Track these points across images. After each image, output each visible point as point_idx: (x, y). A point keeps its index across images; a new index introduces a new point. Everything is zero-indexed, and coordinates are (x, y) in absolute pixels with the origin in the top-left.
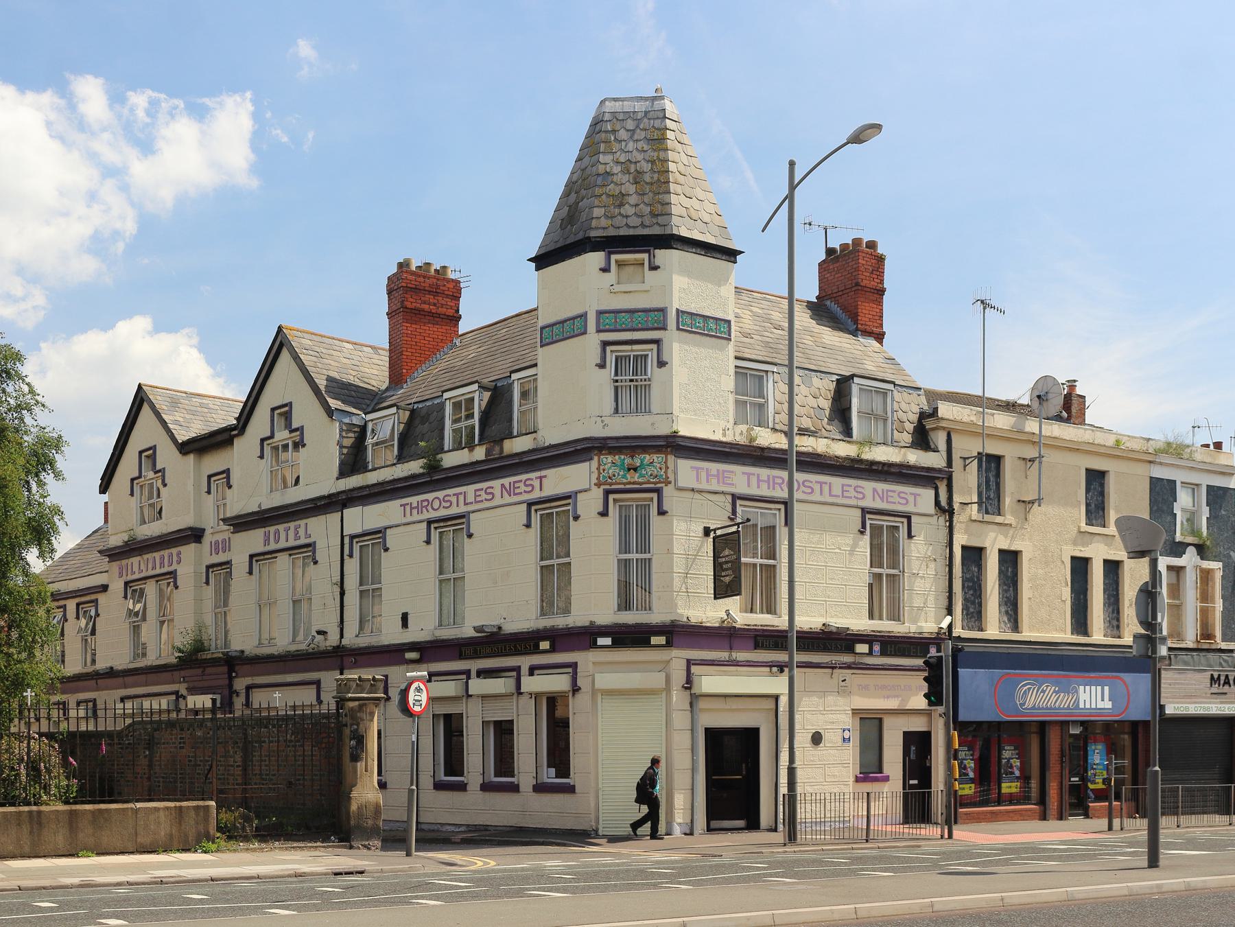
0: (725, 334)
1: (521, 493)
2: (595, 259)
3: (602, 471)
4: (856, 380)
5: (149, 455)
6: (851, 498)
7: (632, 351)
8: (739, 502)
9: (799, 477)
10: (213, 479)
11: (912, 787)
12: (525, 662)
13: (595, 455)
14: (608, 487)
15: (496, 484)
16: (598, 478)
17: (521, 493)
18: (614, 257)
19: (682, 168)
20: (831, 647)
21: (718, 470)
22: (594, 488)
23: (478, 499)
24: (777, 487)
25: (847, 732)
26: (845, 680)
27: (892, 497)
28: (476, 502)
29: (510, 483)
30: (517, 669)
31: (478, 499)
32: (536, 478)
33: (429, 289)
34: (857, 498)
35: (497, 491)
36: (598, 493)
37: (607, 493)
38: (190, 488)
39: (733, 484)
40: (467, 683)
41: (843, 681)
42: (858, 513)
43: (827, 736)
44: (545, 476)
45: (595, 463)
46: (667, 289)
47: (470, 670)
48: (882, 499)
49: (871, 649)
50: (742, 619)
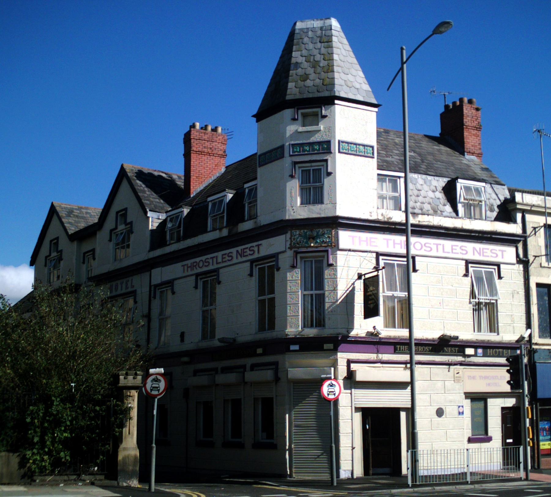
0: (370, 153)
1: (247, 256)
2: (288, 113)
3: (293, 240)
4: (459, 180)
5: (55, 242)
6: (458, 253)
10: (87, 255)
11: (509, 444)
12: (249, 361)
13: (289, 230)
14: (296, 249)
15: (234, 250)
16: (290, 244)
17: (247, 256)
18: (300, 111)
19: (342, 58)
20: (448, 351)
21: (367, 238)
22: (288, 251)
23: (224, 260)
25: (461, 408)
27: (456, 249)
28: (223, 262)
29: (241, 249)
30: (244, 367)
31: (224, 260)
32: (256, 246)
33: (207, 140)
34: (463, 254)
35: (234, 255)
36: (290, 253)
37: (297, 253)
38: (74, 261)
40: (244, 374)
42: (463, 263)
43: (448, 411)
44: (261, 245)
45: (288, 235)
46: (331, 129)
47: (217, 368)
48: (480, 254)
49: (476, 352)
50: (386, 333)
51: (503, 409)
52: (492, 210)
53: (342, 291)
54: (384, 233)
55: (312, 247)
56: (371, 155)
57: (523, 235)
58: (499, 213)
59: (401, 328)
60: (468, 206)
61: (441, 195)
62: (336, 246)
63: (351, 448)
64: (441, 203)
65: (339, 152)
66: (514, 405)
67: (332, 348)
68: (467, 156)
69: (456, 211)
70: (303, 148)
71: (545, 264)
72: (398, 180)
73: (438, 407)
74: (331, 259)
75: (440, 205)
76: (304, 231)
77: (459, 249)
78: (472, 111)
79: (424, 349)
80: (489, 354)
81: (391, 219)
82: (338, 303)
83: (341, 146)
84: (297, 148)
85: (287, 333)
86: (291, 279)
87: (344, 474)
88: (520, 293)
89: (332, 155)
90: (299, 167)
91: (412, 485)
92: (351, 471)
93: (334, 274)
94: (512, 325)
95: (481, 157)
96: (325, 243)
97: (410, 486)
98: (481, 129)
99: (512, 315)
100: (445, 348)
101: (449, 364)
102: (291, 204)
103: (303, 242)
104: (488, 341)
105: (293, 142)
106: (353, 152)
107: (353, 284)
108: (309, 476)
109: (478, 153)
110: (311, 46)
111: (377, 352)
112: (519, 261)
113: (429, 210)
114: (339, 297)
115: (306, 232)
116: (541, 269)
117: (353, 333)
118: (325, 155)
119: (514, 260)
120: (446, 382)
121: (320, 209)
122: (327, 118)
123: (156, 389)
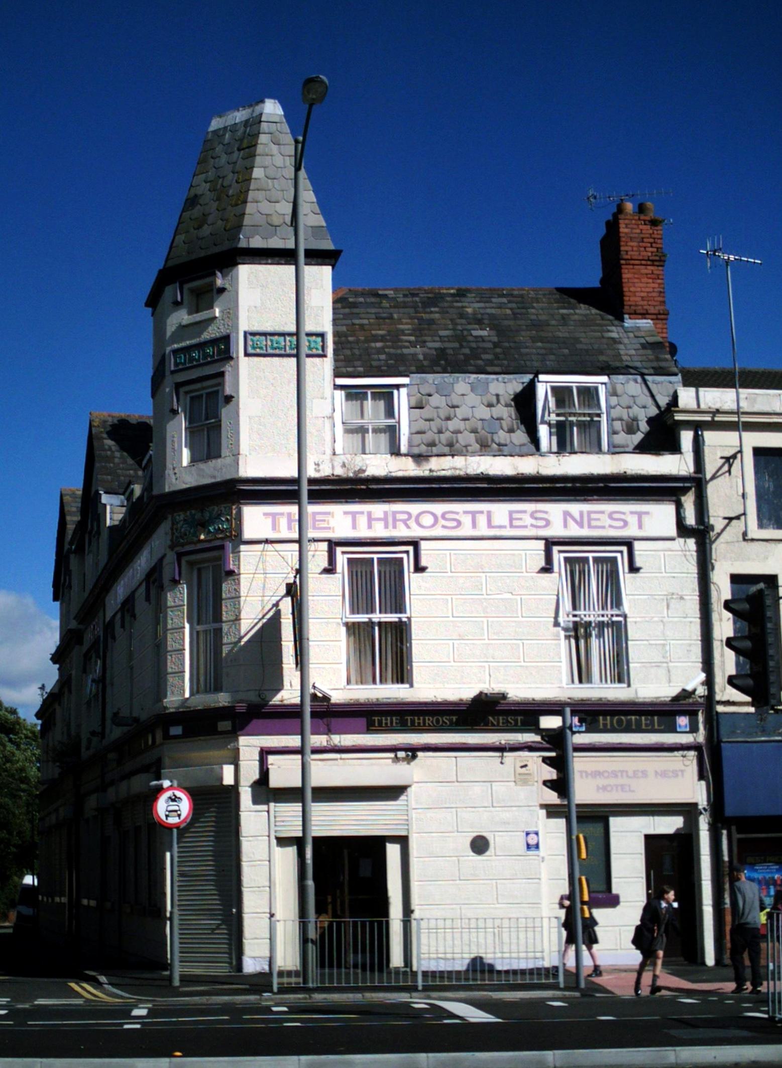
0: (317, 349)
6: (526, 527)
7: (204, 388)
8: (555, 549)
9: (312, 509)
18: (186, 287)
20: (498, 722)
24: (401, 525)
25: (532, 836)
26: (525, 766)
37: (180, 556)
39: (329, 528)
41: (522, 767)
42: (541, 544)
46: (232, 313)
48: (581, 525)
51: (650, 839)
52: (631, 429)
53: (251, 621)
54: (347, 502)
55: (202, 541)
56: (320, 352)
57: (696, 475)
58: (647, 435)
59: (398, 682)
60: (561, 431)
61: (507, 413)
62: (236, 537)
63: (268, 915)
64: (502, 429)
65: (247, 354)
66: (678, 830)
67: (230, 728)
68: (629, 323)
69: (535, 440)
70: (204, 351)
71: (754, 531)
72: (395, 392)
73: (475, 834)
74: (231, 562)
75: (501, 432)
76: (191, 513)
77: (529, 517)
78: (641, 227)
79: (438, 721)
80: (601, 727)
81: (364, 471)
82: (242, 643)
83: (250, 343)
84: (180, 358)
85: (165, 705)
86: (173, 604)
87: (252, 964)
88: (685, 597)
89: (232, 363)
90: (186, 393)
91: (423, 986)
92: (268, 959)
93: (235, 590)
94: (665, 665)
95: (666, 319)
96: (222, 531)
97: (420, 988)
98: (664, 261)
99: (664, 645)
100: (491, 718)
101: (500, 749)
102: (173, 465)
103: (190, 532)
104: (600, 699)
105: (176, 346)
106: (277, 352)
107: (276, 605)
108: (198, 967)
109: (656, 312)
110: (224, 158)
111: (327, 731)
112: (683, 530)
113: (470, 446)
114: (243, 632)
115: (195, 514)
116: (745, 543)
117: (276, 699)
118: (217, 365)
119: (672, 531)
120: (494, 784)
121: (215, 469)
122: (226, 293)
123: (175, 814)
